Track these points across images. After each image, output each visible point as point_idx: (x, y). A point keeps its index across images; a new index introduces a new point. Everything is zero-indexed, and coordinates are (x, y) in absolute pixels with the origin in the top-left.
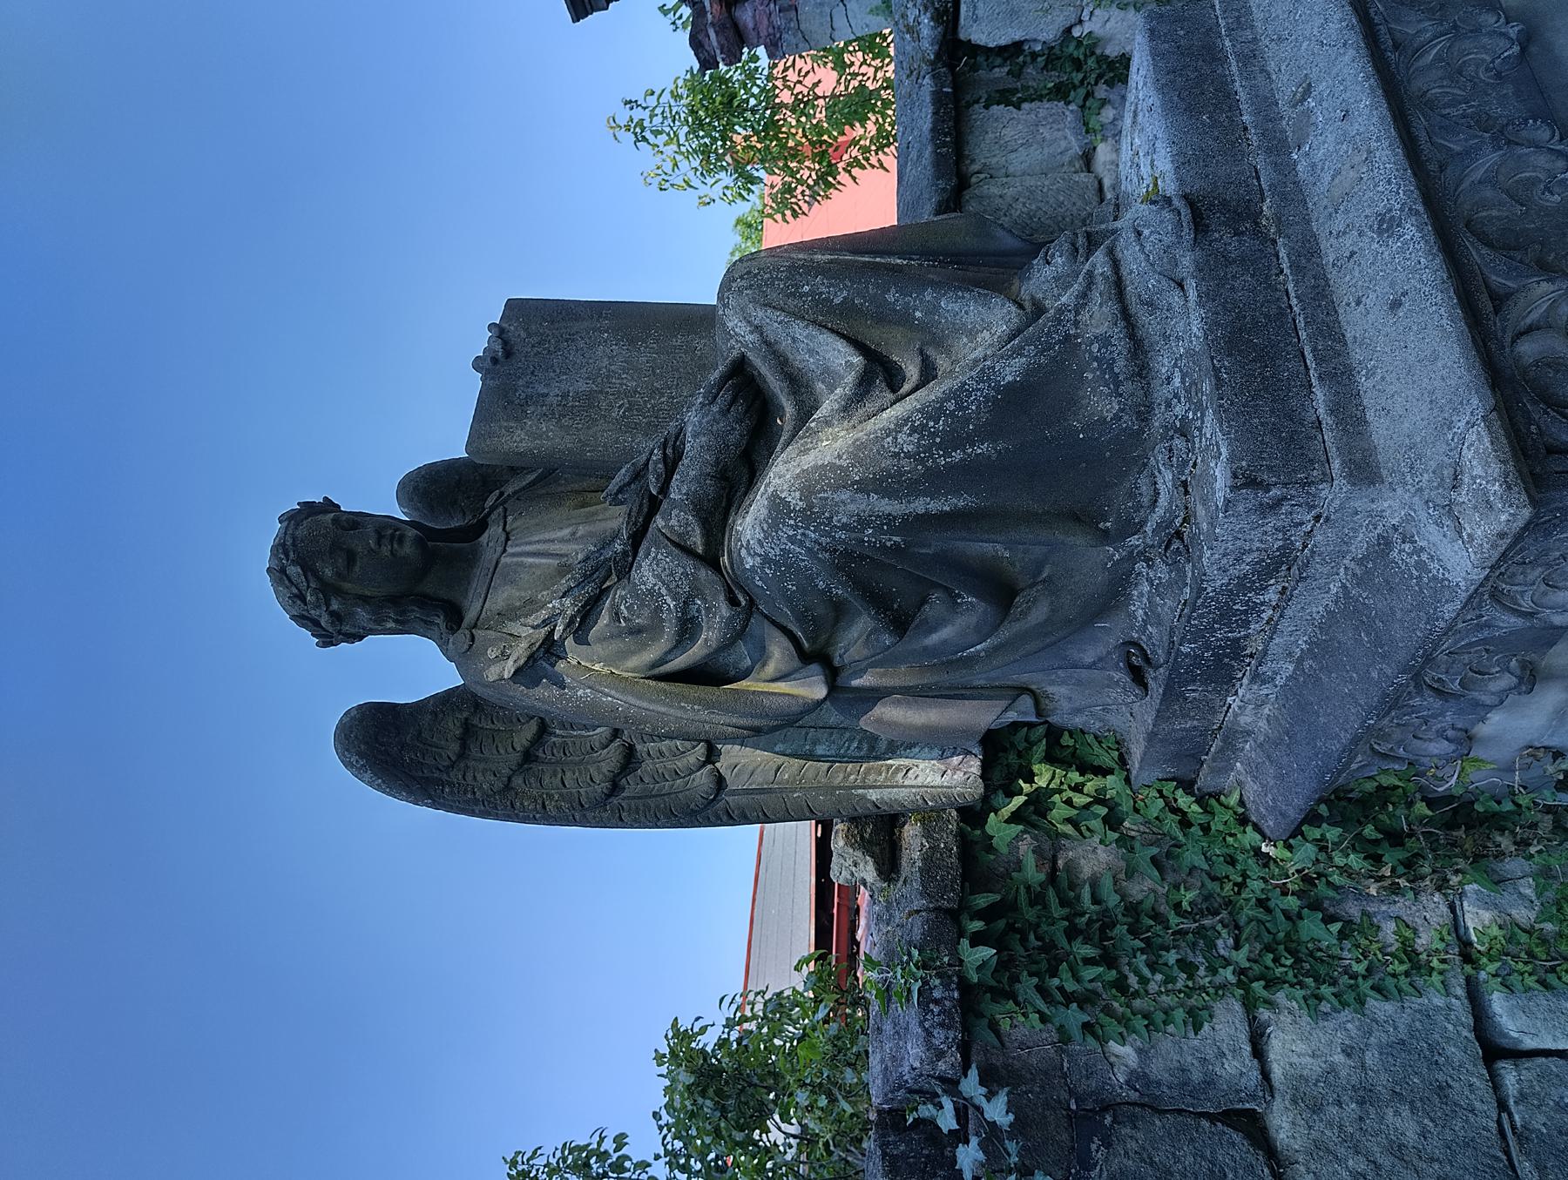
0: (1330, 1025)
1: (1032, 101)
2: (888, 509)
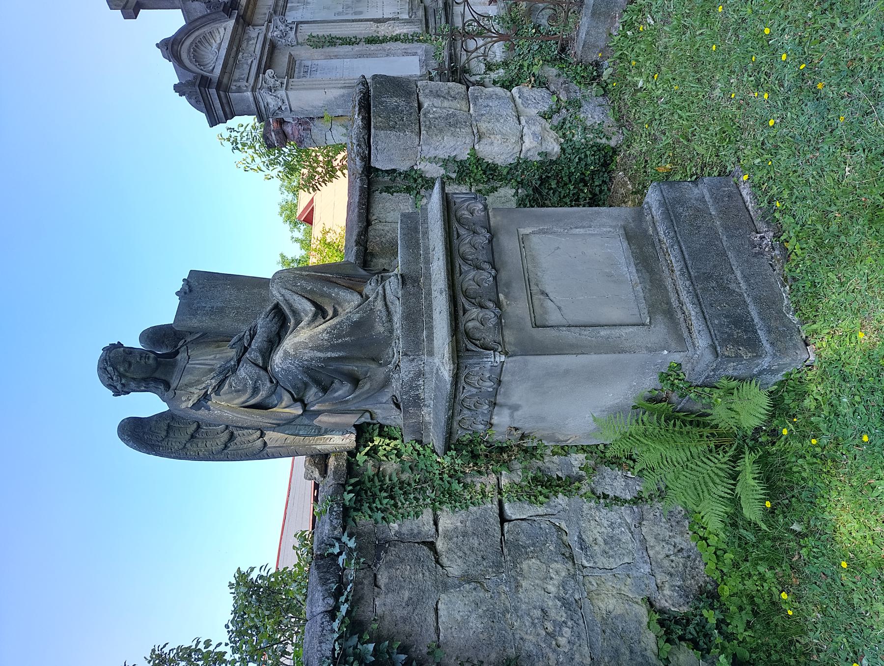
0: (457, 515)
1: (398, 192)
2: (320, 355)
